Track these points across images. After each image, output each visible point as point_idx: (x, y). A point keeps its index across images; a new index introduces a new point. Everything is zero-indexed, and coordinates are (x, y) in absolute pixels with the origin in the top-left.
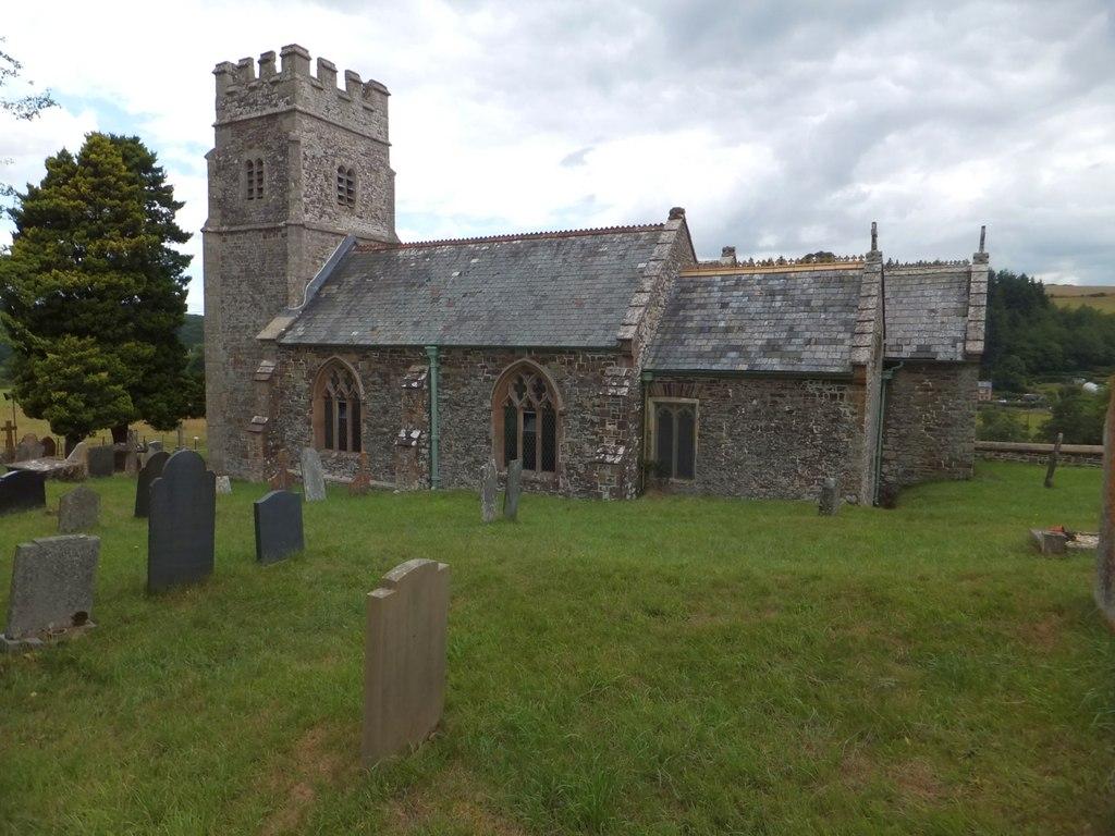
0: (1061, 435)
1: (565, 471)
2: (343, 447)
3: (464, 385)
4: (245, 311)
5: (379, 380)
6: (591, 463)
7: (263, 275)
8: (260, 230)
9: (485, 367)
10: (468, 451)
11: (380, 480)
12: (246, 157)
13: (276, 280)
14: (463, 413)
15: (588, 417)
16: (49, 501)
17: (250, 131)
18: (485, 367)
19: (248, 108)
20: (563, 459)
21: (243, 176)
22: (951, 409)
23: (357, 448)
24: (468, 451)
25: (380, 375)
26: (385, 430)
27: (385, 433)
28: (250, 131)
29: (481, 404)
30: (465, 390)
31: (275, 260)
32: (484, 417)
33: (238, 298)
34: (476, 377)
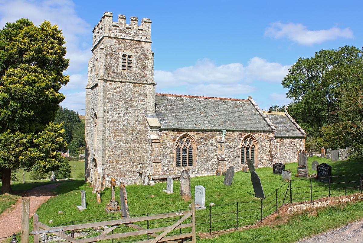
0: (361, 178)
1: (259, 162)
2: (184, 165)
3: (232, 141)
4: (122, 115)
5: (203, 141)
6: (265, 160)
7: (133, 101)
8: (132, 83)
9: (238, 136)
10: (233, 161)
11: (204, 174)
12: (123, 53)
13: (140, 103)
14: (232, 149)
15: (264, 148)
16: (177, 167)
17: (126, 44)
18: (238, 136)
19: (125, 35)
20: (259, 159)
21: (121, 59)
22: (329, 120)
23: (191, 164)
24: (233, 161)
25: (204, 139)
26: (205, 157)
27: (205, 158)
28: (126, 44)
29: (237, 146)
30: (232, 143)
31: (140, 95)
32: (238, 150)
33: (118, 109)
34: (236, 139)
